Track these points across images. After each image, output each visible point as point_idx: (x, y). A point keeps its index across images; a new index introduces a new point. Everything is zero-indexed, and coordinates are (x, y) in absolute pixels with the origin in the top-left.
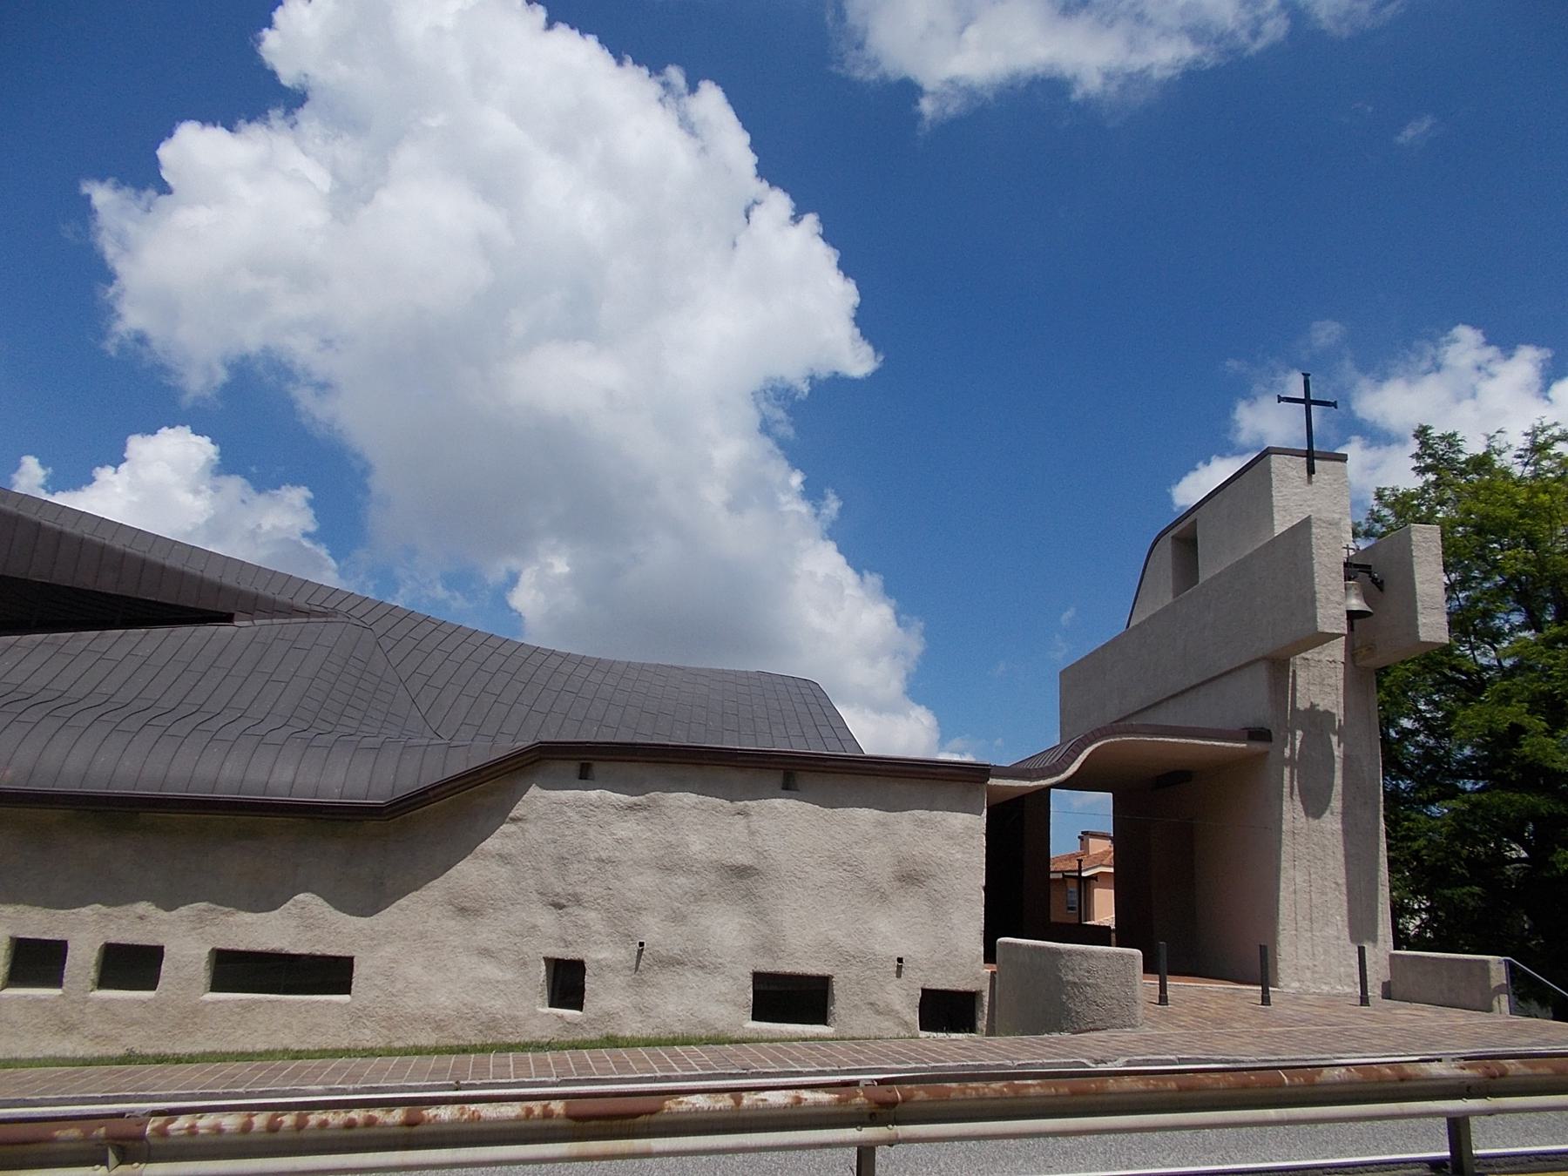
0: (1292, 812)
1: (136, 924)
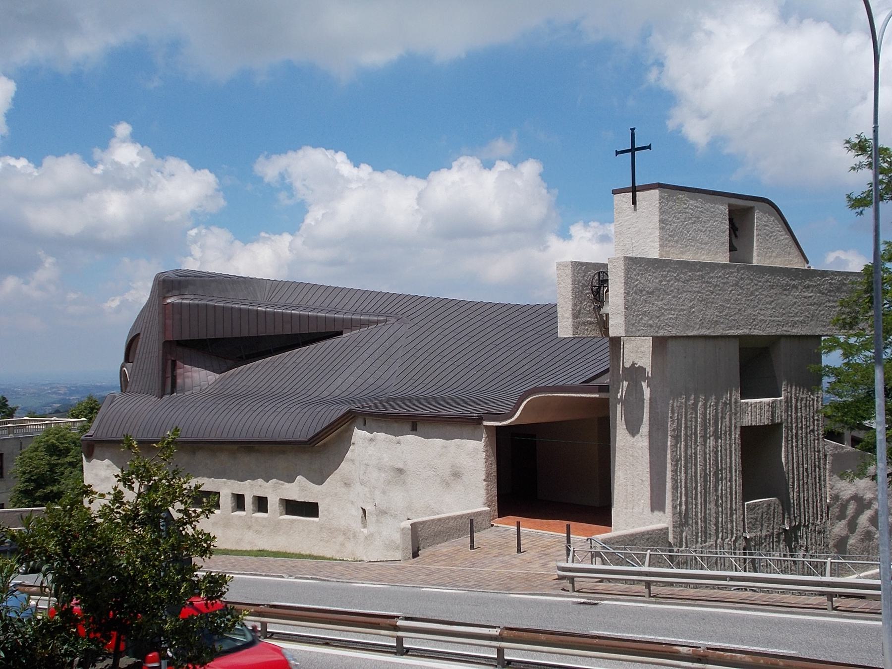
0: (621, 437)
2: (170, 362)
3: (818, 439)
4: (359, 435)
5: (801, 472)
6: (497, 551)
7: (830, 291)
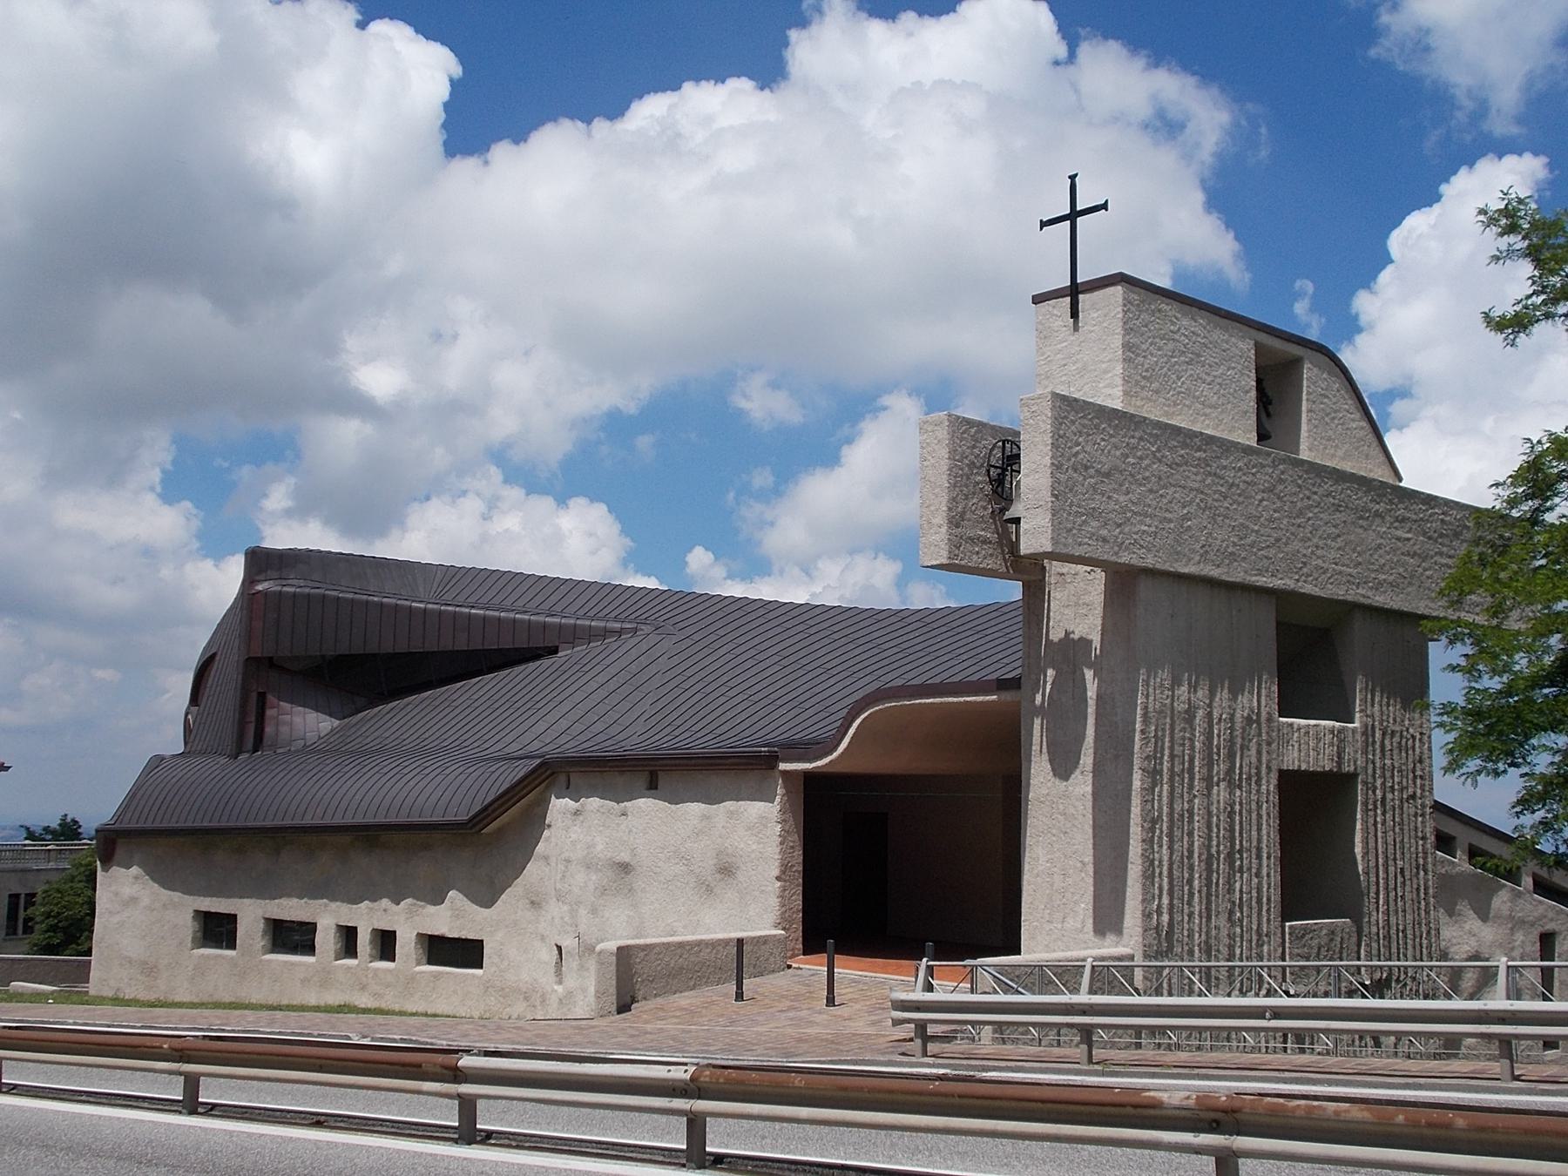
0: (1039, 773)
1: (292, 909)
2: (254, 696)
3: (1423, 815)
4: (559, 806)
5: (1391, 875)
6: (788, 1003)
7: (1441, 535)
